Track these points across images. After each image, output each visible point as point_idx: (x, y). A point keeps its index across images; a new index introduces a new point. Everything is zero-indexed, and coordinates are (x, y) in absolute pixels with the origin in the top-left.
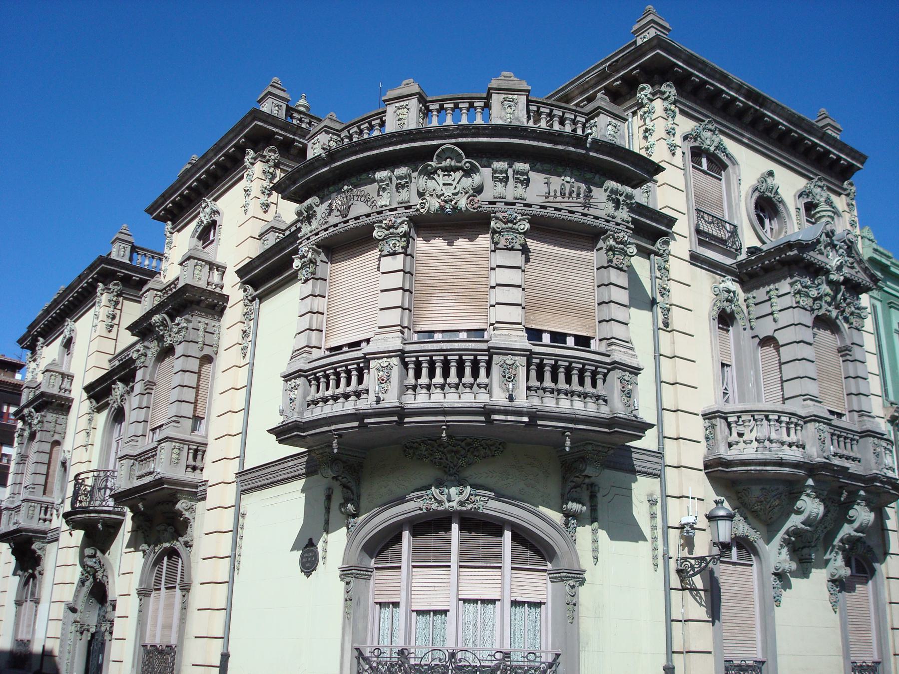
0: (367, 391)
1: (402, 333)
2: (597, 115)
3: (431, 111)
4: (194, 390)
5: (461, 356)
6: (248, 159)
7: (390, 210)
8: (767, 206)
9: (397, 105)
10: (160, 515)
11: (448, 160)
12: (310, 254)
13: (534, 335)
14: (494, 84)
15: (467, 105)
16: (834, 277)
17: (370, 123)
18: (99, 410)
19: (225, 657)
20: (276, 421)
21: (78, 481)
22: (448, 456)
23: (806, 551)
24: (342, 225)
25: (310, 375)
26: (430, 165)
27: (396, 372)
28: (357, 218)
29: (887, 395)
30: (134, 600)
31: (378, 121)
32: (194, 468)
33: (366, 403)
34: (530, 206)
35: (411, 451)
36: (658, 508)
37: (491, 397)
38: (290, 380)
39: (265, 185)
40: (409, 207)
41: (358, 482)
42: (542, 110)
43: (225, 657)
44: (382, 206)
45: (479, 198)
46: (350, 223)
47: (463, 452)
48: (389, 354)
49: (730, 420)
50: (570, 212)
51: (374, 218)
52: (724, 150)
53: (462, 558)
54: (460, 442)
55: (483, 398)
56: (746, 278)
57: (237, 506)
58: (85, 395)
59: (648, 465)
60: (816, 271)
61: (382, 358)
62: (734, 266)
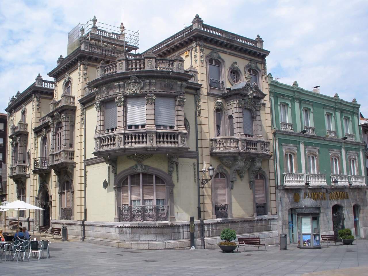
0: (116, 144)
2: (175, 61)
4: (270, 172)
5: (139, 134)
6: (79, 63)
10: (65, 173)
12: (99, 105)
13: (158, 127)
16: (250, 97)
17: (113, 66)
18: (38, 137)
19: (86, 210)
20: (94, 151)
21: (35, 160)
23: (241, 174)
28: (110, 96)
29: (273, 126)
30: (58, 195)
32: (72, 159)
33: (116, 147)
36: (196, 167)
40: (124, 93)
41: (116, 165)
43: (86, 210)
45: (142, 90)
47: (141, 157)
48: (121, 134)
49: (217, 141)
52: (220, 58)
53: (143, 183)
55: (145, 145)
56: (225, 98)
57: (85, 169)
58: (33, 132)
60: (246, 95)
62: (222, 94)
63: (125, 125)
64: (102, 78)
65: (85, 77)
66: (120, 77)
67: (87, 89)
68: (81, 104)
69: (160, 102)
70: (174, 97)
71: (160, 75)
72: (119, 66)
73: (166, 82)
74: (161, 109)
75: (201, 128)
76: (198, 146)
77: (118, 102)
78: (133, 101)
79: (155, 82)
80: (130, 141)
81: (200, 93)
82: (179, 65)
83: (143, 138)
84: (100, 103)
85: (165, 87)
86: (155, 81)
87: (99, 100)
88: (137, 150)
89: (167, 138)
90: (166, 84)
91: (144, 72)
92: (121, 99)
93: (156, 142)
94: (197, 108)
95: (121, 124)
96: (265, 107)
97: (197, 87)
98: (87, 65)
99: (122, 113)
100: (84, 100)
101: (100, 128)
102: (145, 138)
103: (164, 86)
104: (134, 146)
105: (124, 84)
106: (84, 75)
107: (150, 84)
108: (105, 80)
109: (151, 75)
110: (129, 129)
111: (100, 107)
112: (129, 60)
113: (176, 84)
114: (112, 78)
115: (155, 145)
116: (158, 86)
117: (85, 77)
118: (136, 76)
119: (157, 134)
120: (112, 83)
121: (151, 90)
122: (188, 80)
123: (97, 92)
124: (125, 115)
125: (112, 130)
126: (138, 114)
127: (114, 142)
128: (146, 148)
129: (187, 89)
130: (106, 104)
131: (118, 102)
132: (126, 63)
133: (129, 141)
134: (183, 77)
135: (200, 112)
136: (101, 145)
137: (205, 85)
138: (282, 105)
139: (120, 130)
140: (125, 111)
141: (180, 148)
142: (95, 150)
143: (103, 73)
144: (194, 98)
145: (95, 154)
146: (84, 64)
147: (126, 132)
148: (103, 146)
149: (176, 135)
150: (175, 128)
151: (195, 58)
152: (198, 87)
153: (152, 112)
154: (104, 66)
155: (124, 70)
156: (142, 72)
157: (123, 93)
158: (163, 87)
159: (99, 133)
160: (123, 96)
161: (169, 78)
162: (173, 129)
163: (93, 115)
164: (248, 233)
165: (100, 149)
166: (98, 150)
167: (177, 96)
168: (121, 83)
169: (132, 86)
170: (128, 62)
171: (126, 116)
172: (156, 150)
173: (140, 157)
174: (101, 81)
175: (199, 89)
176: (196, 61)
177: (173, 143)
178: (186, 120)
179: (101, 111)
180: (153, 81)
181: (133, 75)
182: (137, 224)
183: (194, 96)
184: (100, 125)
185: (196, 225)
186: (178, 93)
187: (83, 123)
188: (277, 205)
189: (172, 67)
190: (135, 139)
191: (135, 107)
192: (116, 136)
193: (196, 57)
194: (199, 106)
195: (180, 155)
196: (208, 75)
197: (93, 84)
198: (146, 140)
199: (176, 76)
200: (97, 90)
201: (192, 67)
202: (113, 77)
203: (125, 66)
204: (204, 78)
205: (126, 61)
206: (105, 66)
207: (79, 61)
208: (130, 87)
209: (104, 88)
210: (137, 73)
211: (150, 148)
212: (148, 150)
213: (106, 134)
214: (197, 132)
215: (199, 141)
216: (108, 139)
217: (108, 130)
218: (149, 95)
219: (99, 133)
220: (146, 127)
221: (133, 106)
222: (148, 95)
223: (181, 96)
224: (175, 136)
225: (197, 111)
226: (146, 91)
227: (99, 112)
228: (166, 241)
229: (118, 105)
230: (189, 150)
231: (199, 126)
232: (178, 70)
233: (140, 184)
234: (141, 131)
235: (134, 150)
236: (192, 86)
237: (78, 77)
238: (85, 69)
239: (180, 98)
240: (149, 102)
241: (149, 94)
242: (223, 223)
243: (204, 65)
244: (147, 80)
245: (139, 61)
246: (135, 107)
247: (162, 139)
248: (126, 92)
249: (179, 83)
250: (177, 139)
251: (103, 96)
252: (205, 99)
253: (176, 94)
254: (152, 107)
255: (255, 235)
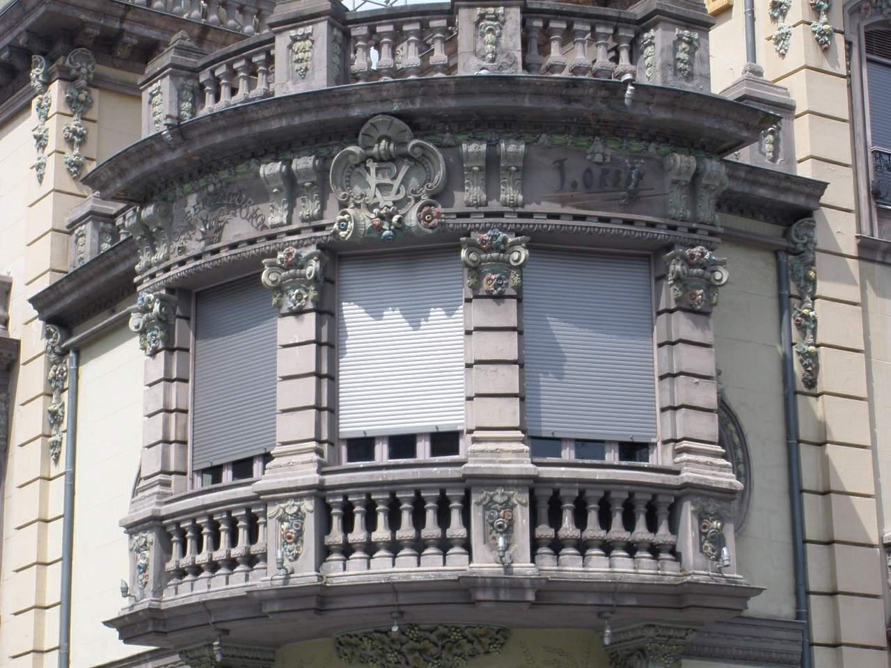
0: (264, 556)
1: (319, 452)
2: (654, 25)
3: (356, 39)
6: (36, 73)
7: (290, 233)
9: (293, 33)
11: (383, 142)
12: (157, 307)
13: (543, 445)
15: (417, 27)
20: (119, 606)
22: (410, 658)
24: (209, 258)
25: (170, 524)
26: (351, 153)
27: (310, 524)
28: (233, 246)
31: (263, 57)
33: (264, 579)
35: (348, 651)
37: (471, 560)
38: (136, 533)
39: (72, 127)
40: (322, 228)
42: (553, 25)
44: (274, 226)
45: (440, 209)
46: (223, 254)
47: (434, 650)
48: (297, 492)
50: (601, 219)
51: (262, 246)
54: (428, 634)
55: (457, 563)
61: (287, 499)
63: (325, 436)
64: (179, 129)
65: (72, 155)
66: (297, 121)
67: (88, 228)
68: (49, 321)
69: (555, 280)
70: (648, 255)
71: (557, 106)
72: (289, 58)
73: (599, 158)
74: (566, 334)
75: (825, 463)
76: (805, 583)
77: (280, 289)
78: (385, 279)
79: (526, 157)
80: (358, 535)
81: (811, 240)
82: (675, 50)
83: (444, 521)
84: (163, 300)
85: (587, 186)
86: (522, 147)
87: (161, 277)
88: (402, 599)
89: (605, 523)
90: (597, 172)
91: (452, 89)
92: (298, 263)
93: (535, 544)
94: (795, 334)
95: (303, 426)
97: (790, 199)
98: (91, 85)
99: (306, 359)
100: (68, 293)
101: (165, 458)
102: (456, 517)
103: (579, 181)
104: (382, 566)
105: (322, 171)
106: (70, 142)
107: (492, 164)
108: (198, 146)
109: (487, 112)
110: (350, 459)
111: (164, 322)
112: (358, 21)
113: (661, 168)
114: (245, 131)
115: (523, 567)
116: (547, 177)
117: (72, 155)
118: (398, 115)
119: (537, 492)
120: (241, 168)
121: (494, 206)
122: (740, 144)
123: (143, 226)
124: (325, 370)
125: (243, 468)
126: (417, 366)
127: (255, 549)
128: (464, 590)
129: (730, 210)
130: (211, 300)
131: (280, 289)
132: (332, 40)
133: (352, 537)
134: (709, 123)
135: (811, 360)
136: (170, 566)
137: (842, 190)
139: (295, 469)
140: (329, 345)
141: (694, 588)
142: (127, 602)
143: (187, 105)
144: (771, 274)
145: (128, 627)
146: (69, 79)
147: (331, 480)
148: (181, 573)
149: (665, 500)
150: (660, 457)
151: (774, 19)
152: (801, 201)
153: (507, 346)
154: (192, 61)
155: (319, 81)
156: (442, 89)
157: (317, 229)
158: (574, 185)
159: (157, 489)
160: (313, 249)
161: (617, 129)
162: (645, 464)
163: (122, 382)
165: (158, 592)
166: (146, 602)
167: (669, 247)
168: (303, 163)
169: (372, 179)
170: (347, 35)
171: (333, 378)
172: (531, 597)
173: (422, 651)
174: (170, 157)
175: (807, 213)
176: (781, 39)
177: (644, 556)
178: (725, 412)
179: (170, 349)
180: (512, 148)
181: (380, 108)
183: (770, 258)
184: (166, 441)
186: (674, 228)
187: (57, 444)
189: (632, 60)
190: (394, 523)
191: (393, 316)
192: (265, 504)
193: (783, 14)
194: (808, 325)
195: (692, 637)
196: (859, 129)
197: (122, 173)
198: (462, 532)
199: (662, 115)
200: (149, 211)
201: (760, 74)
202: (250, 122)
203: (330, 54)
204: (839, 143)
205: (331, 26)
206: (201, 63)
207: (36, 58)
208: (357, 190)
209: (192, 200)
210: (404, 98)
211: (494, 584)
212: (480, 596)
213: (195, 497)
214: (795, 491)
215: (814, 555)
216: (215, 527)
217: (215, 472)
218: (486, 236)
219: (157, 489)
220: (465, 445)
221: (378, 316)
222: (476, 237)
223: (697, 250)
224: (658, 506)
225: (796, 359)
226: (467, 215)
227: (161, 355)
229: (279, 306)
230: (756, 606)
231: (807, 456)
232: (670, 78)
234: (436, 472)
235: (388, 599)
236: (762, 192)
237: (31, 154)
238: (77, 105)
239: (689, 262)
240: (486, 286)
241: (485, 230)
243: (835, 63)
244: (469, 141)
245: (417, 27)
246: (393, 316)
247: (568, 528)
248: (333, 216)
249: (682, 161)
250: (673, 529)
251: (182, 250)
252: (845, 278)
253: (661, 233)
254: (507, 314)
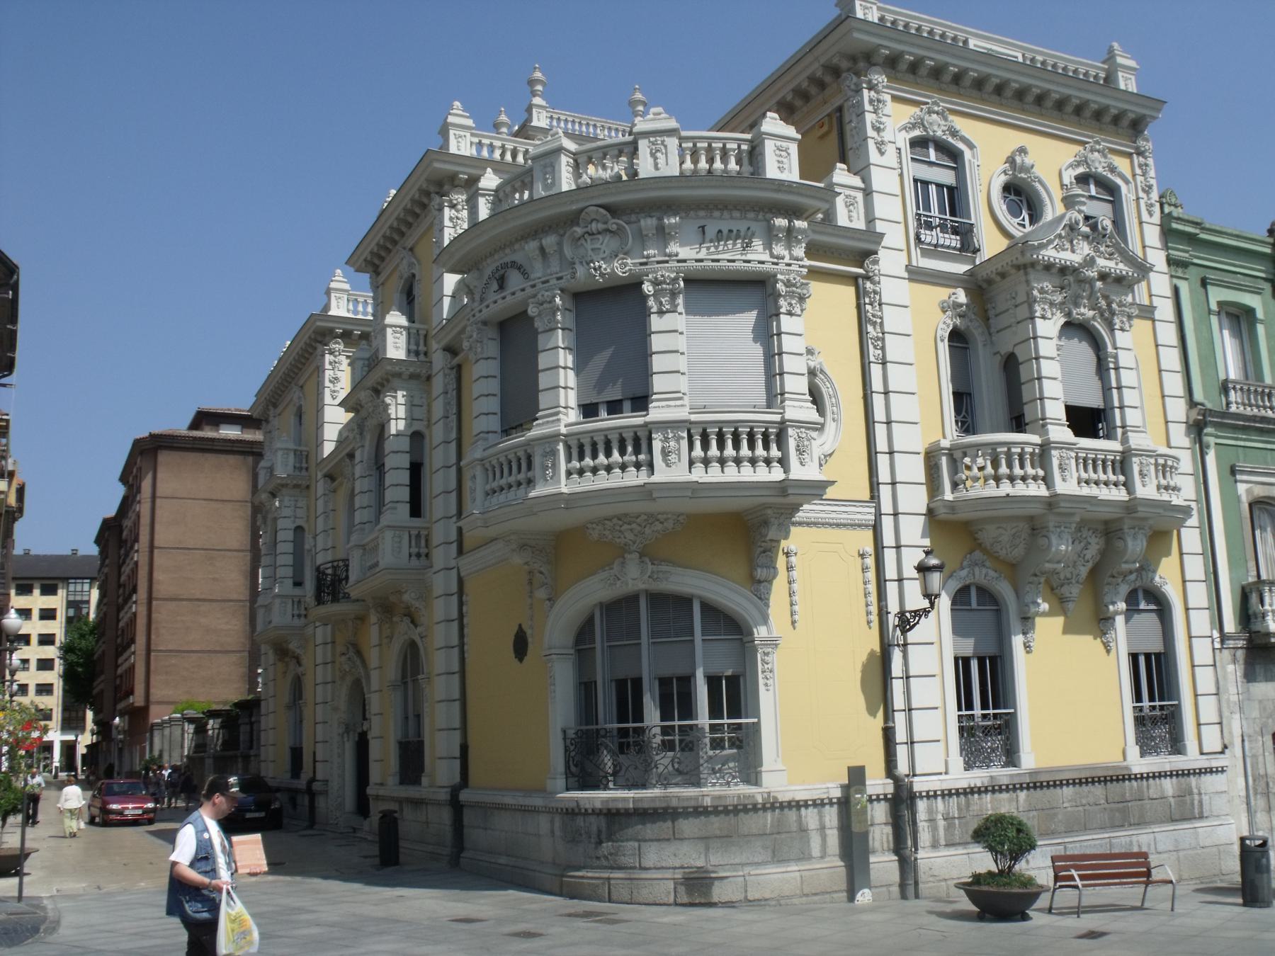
4: (1187, 578)
5: (752, 428)
8: (1021, 194)
14: (641, 125)
19: (464, 749)
27: (684, 443)
34: (685, 261)
43: (464, 749)
50: (713, 261)
52: (954, 133)
53: (654, 634)
59: (834, 515)
96: (1154, 320)
138: (1228, 314)
164: (1103, 828)
182: (625, 799)
185: (878, 800)
188: (1226, 713)
228: (747, 870)
233: (639, 638)
242: (993, 791)
244: (669, 217)
255: (1134, 838)
